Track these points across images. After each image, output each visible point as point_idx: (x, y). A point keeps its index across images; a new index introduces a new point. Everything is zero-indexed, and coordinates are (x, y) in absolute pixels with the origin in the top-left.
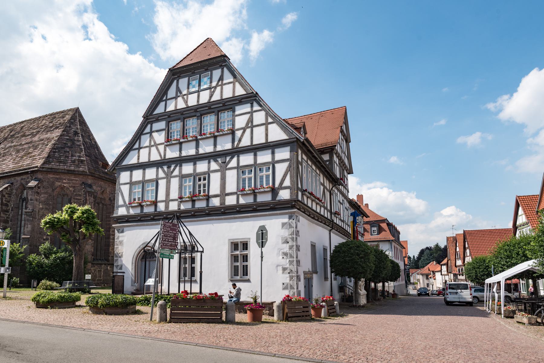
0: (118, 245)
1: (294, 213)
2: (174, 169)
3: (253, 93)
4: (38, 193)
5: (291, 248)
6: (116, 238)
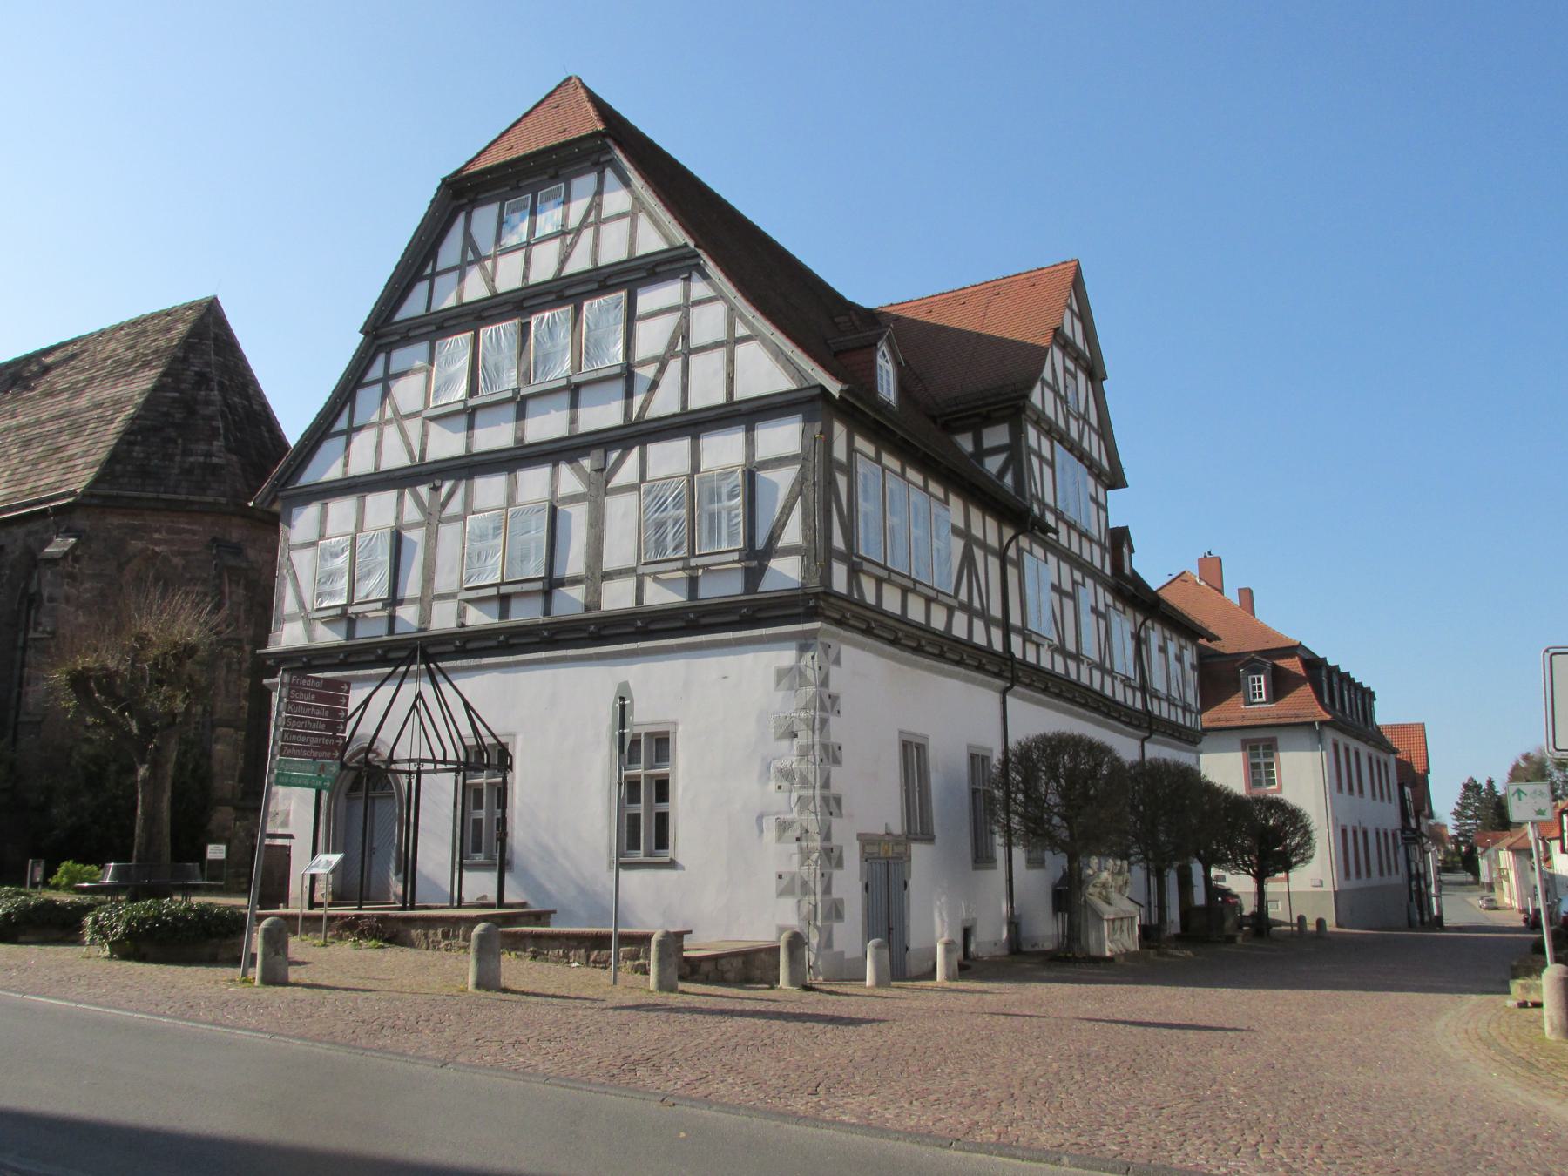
1: (813, 634)
2: (450, 495)
4: (72, 577)
5: (804, 753)
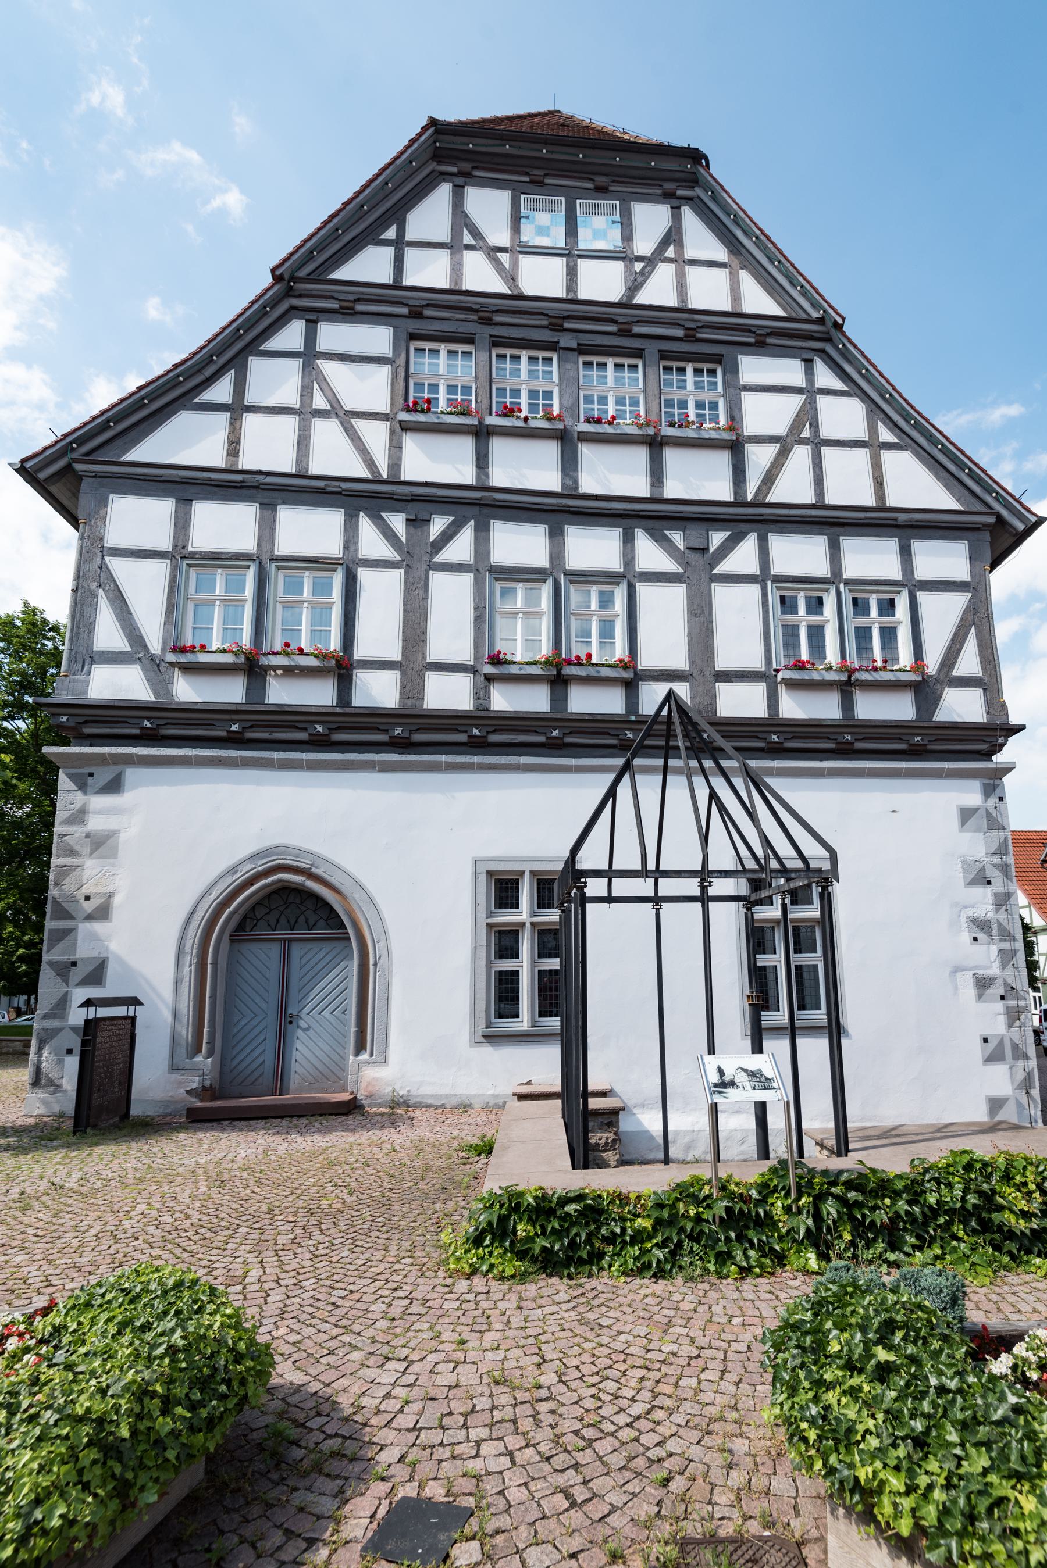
0: (73, 853)
2: (447, 536)
3: (821, 321)
6: (60, 816)
